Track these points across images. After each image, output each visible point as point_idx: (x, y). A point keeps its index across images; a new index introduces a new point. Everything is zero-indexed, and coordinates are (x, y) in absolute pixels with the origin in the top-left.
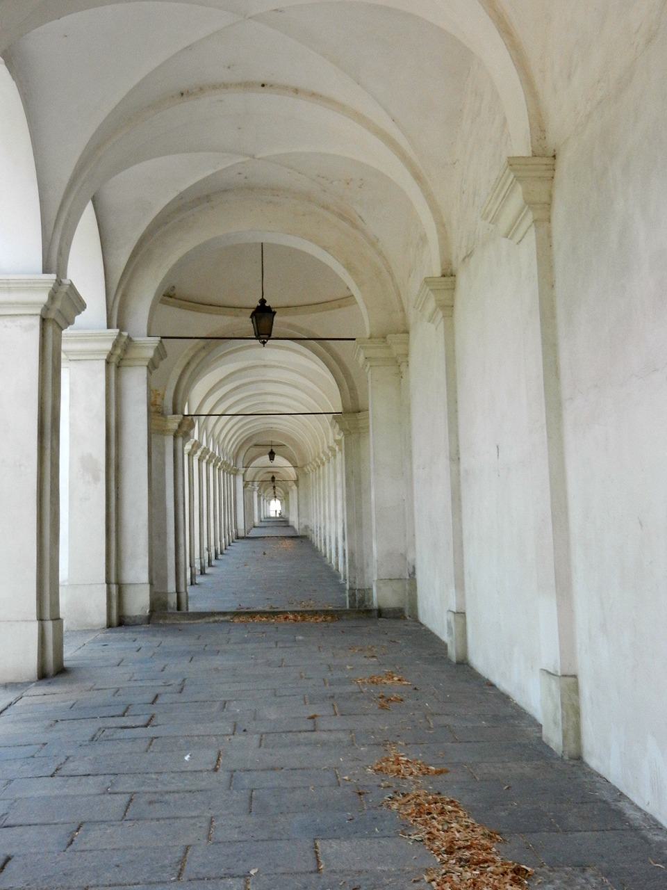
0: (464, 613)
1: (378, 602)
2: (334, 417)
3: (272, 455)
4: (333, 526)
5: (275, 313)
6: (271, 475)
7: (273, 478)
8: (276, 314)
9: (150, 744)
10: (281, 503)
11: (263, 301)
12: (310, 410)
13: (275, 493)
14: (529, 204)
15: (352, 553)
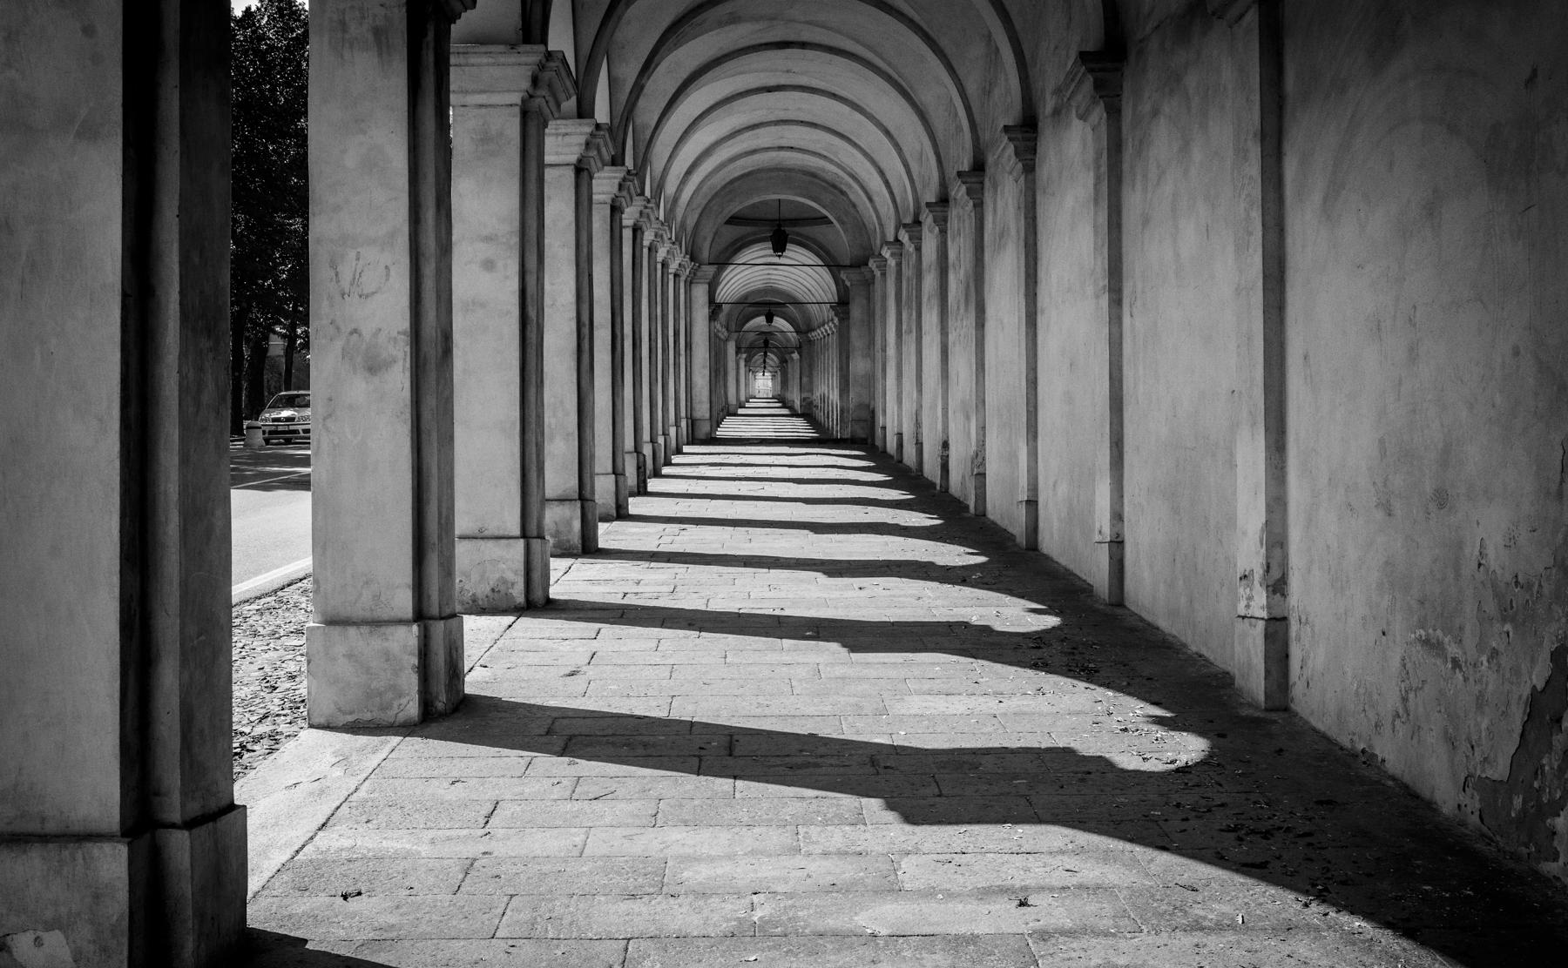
3: (770, 319)
10: (774, 377)
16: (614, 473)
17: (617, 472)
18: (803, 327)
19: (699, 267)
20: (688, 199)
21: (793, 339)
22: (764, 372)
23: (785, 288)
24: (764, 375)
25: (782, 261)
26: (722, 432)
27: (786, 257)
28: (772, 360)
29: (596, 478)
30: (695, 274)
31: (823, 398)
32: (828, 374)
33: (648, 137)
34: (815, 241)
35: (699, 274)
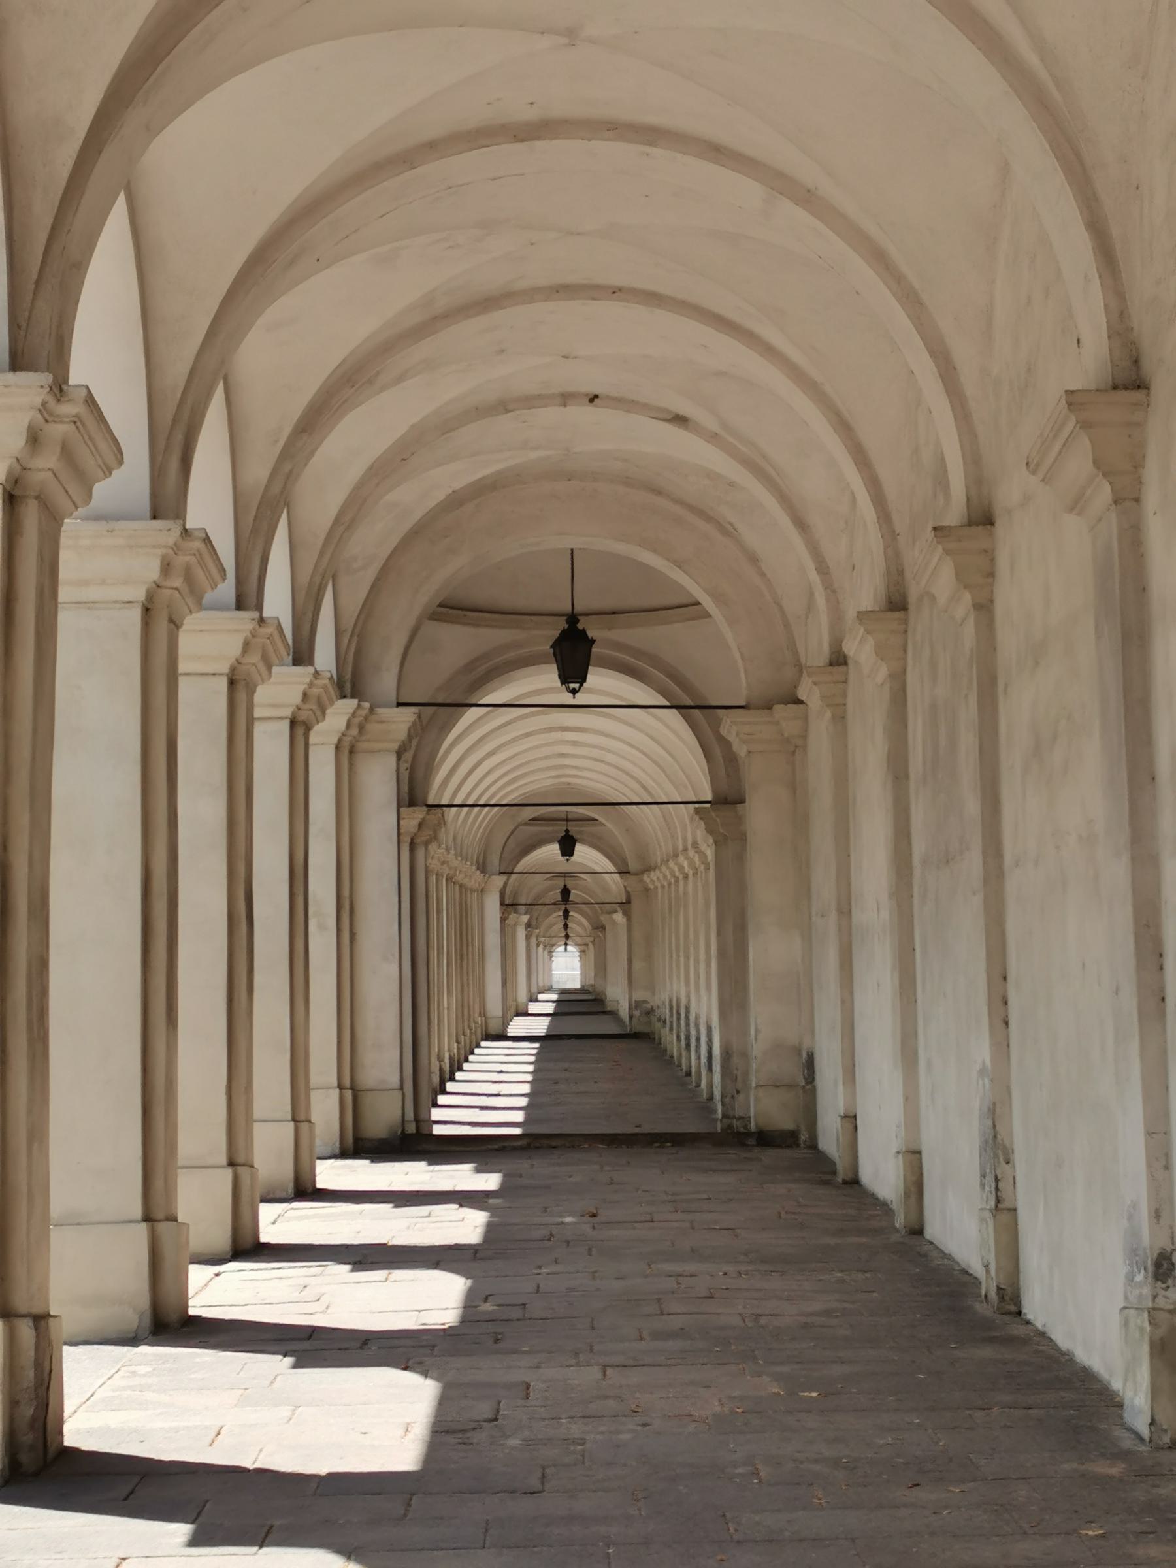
0: (1015, 1210)
1: (756, 1125)
2: (697, 811)
3: (567, 845)
4: (704, 999)
5: (593, 641)
6: (560, 883)
7: (566, 892)
8: (595, 643)
9: (242, 1370)
10: (583, 953)
11: (565, 886)
12: (640, 809)
13: (566, 926)
14: (834, 717)
15: (727, 1053)
16: (294, 1120)
17: (299, 1117)
18: (633, 865)
19: (372, 710)
20: (329, 524)
21: (613, 887)
22: (566, 944)
23: (598, 786)
24: (566, 950)
25: (581, 699)
26: (512, 1031)
27: (591, 691)
28: (580, 924)
29: (256, 1125)
30: (361, 728)
31: (680, 1011)
32: (687, 958)
33: (64, 172)
34: (655, 661)
35: (372, 727)
